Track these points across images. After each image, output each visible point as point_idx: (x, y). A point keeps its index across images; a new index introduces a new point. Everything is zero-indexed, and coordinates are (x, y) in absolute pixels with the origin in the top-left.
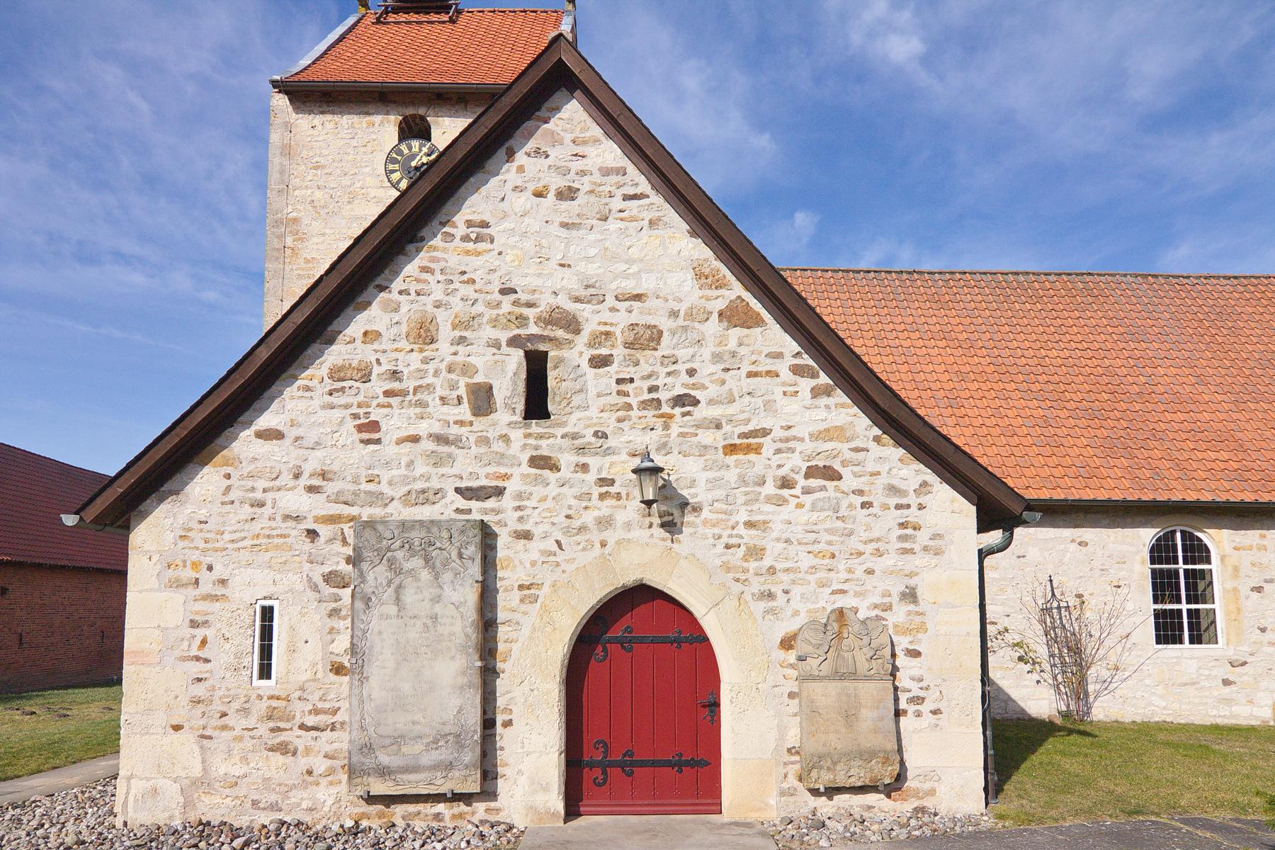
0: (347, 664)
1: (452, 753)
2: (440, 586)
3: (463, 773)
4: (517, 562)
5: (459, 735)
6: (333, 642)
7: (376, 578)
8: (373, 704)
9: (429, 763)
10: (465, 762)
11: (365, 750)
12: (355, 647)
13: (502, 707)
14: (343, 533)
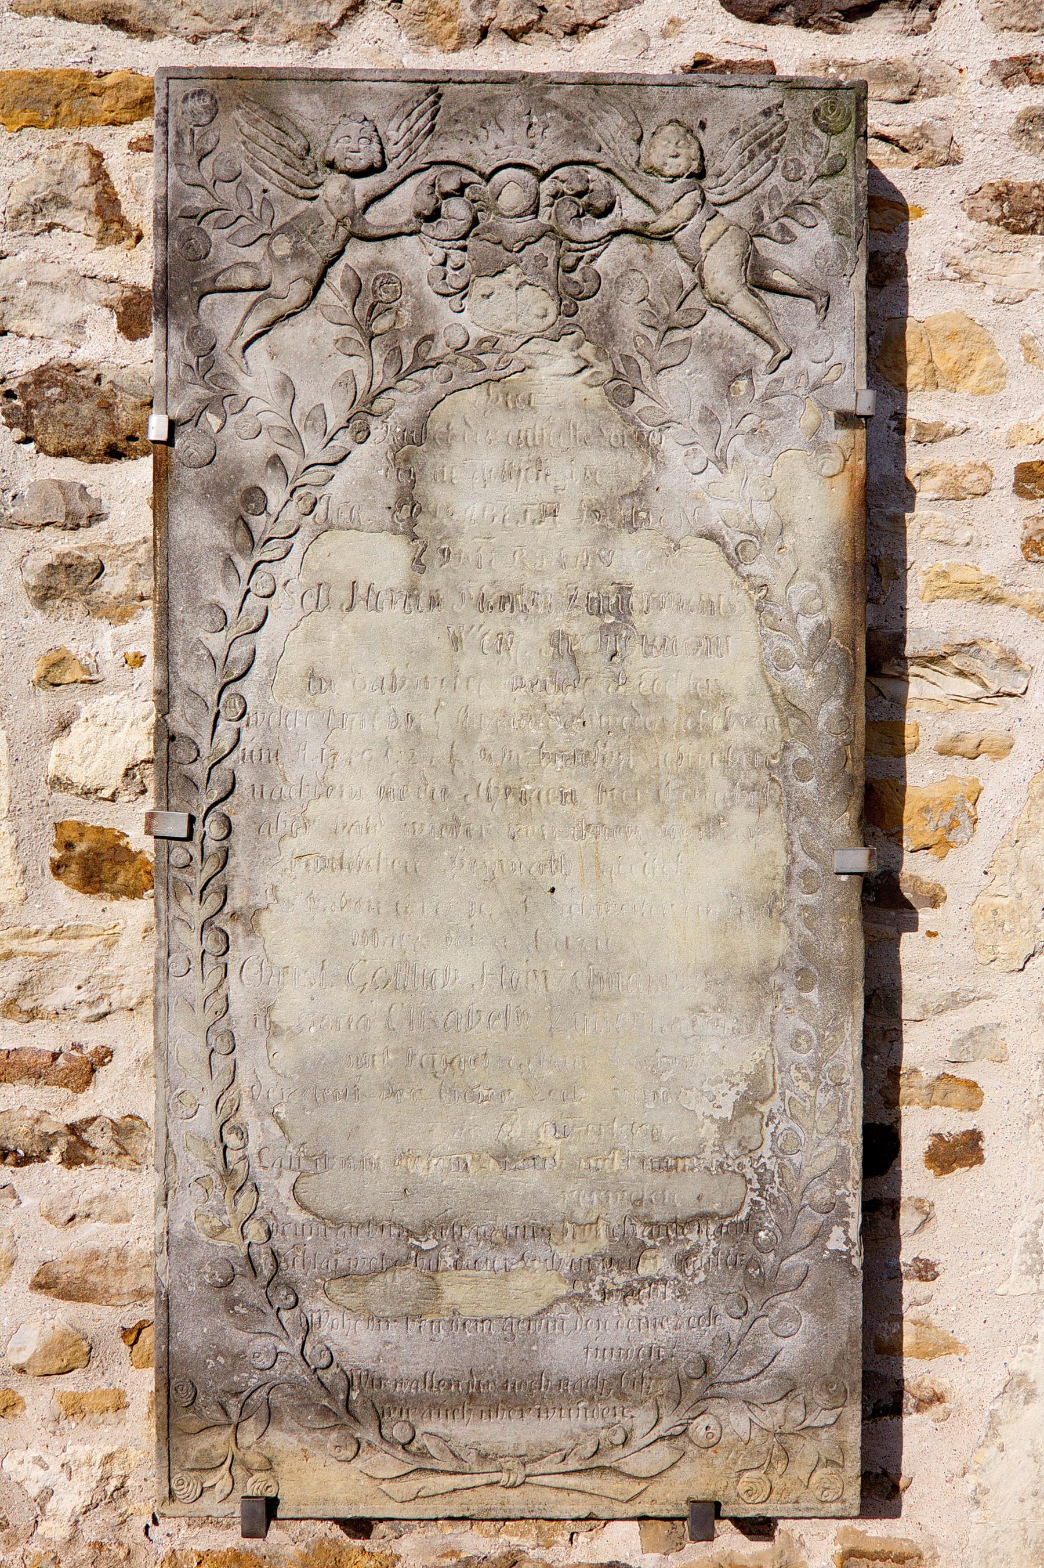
0: (139, 841)
1: (712, 1316)
2: (640, 441)
3: (771, 1417)
4: (1010, 353)
5: (749, 1227)
6: (65, 726)
7: (287, 387)
8: (283, 1052)
9: (591, 1365)
10: (783, 1362)
11: (246, 1289)
12: (182, 753)
13: (928, 1073)
14: (99, 174)
